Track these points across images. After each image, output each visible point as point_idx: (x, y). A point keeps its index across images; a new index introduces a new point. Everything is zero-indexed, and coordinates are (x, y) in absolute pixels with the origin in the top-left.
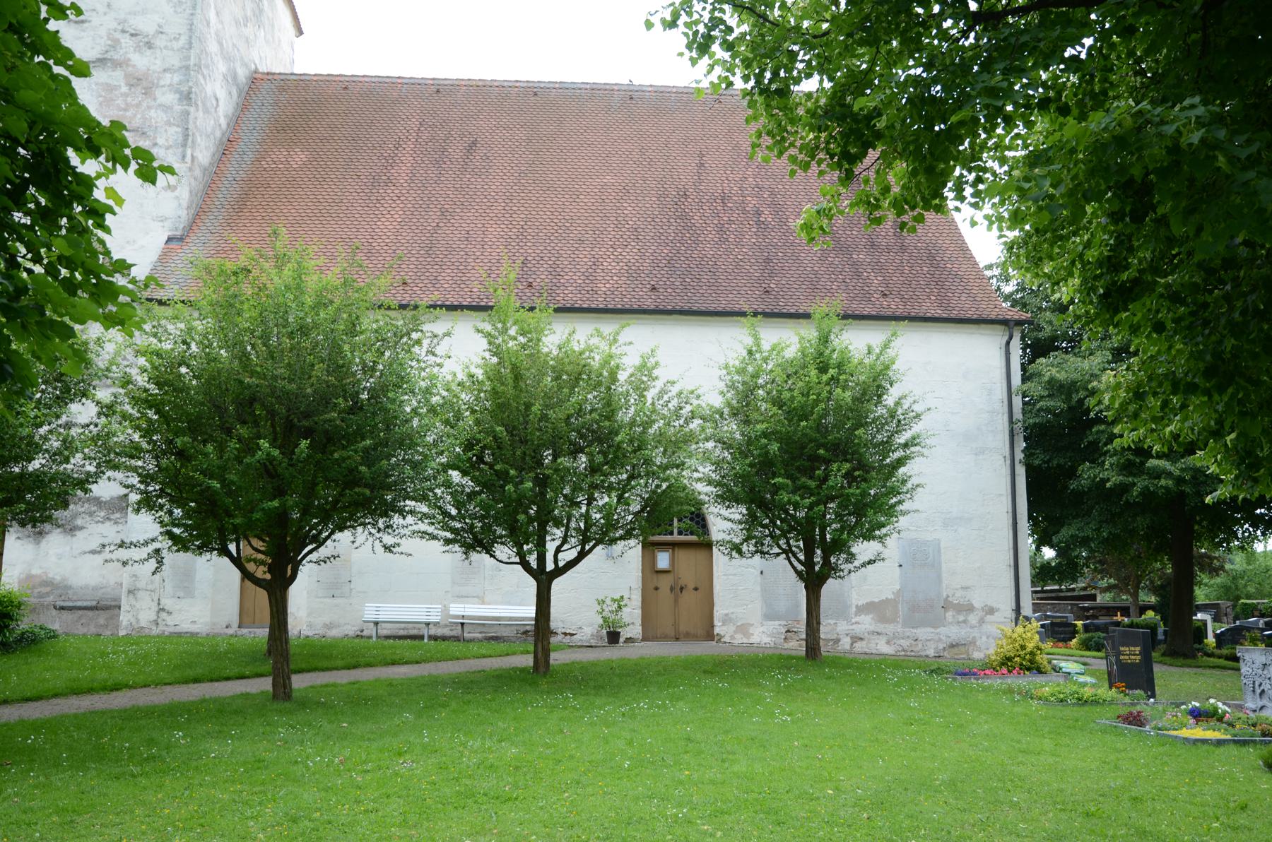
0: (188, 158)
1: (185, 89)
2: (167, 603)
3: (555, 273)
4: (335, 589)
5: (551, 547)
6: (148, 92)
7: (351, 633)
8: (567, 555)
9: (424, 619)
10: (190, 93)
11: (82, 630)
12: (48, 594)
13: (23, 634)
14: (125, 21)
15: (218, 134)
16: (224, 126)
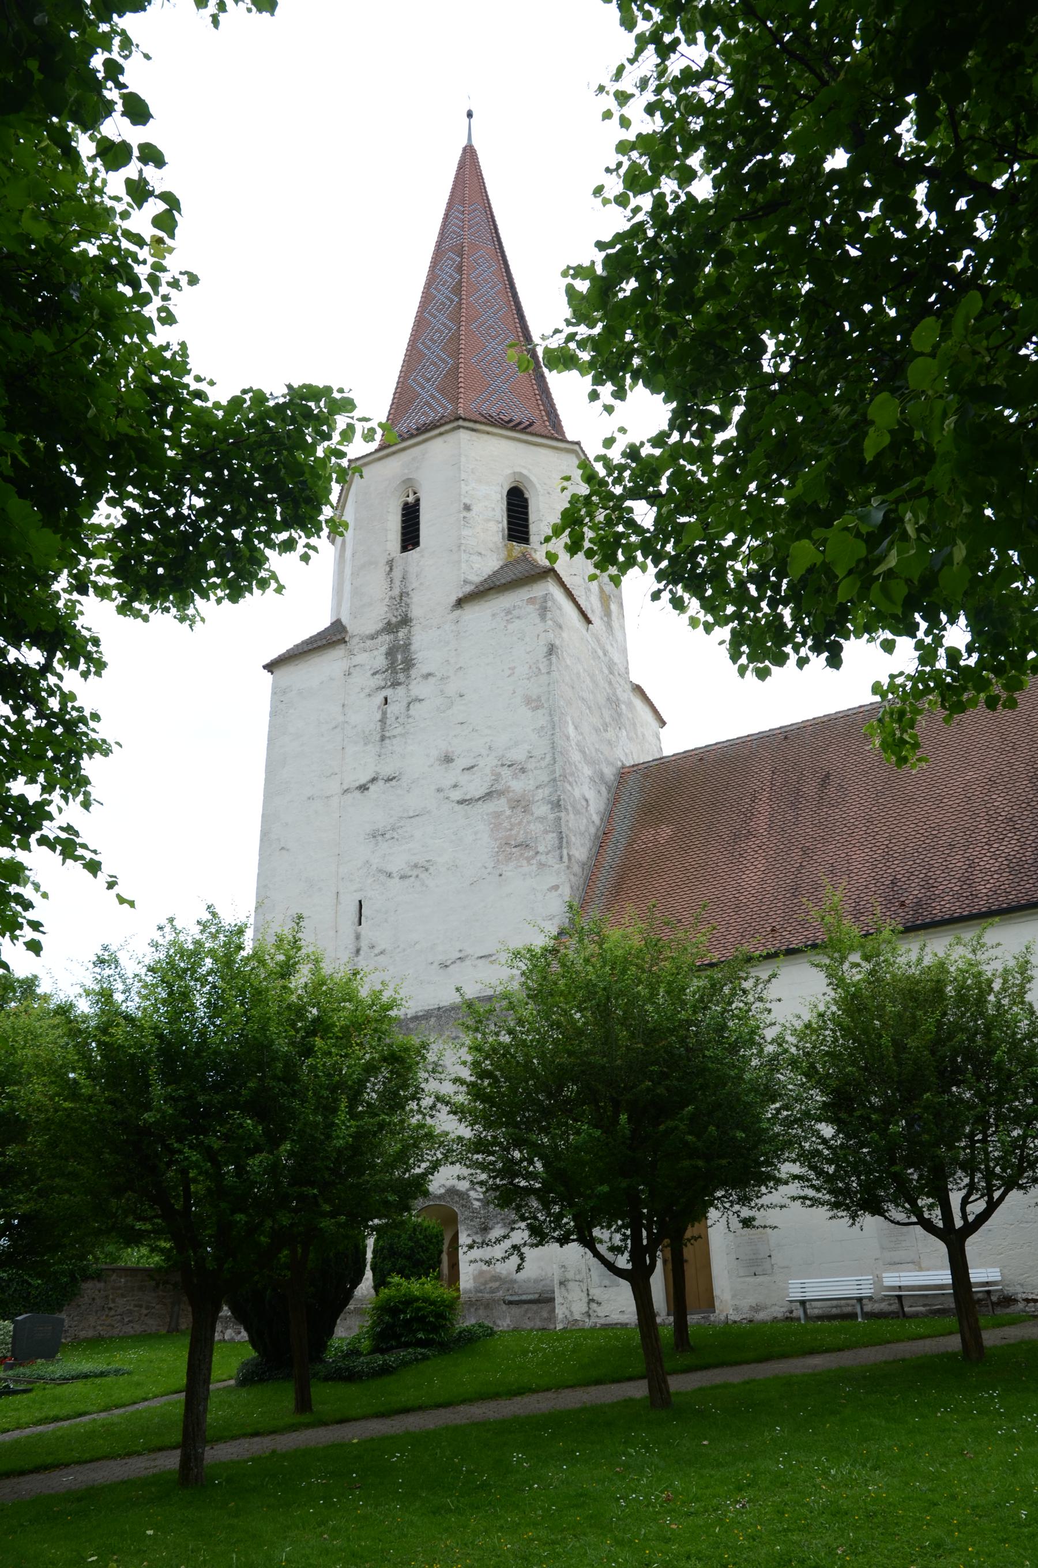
0: (565, 858)
1: (554, 798)
2: (596, 1293)
3: (928, 885)
4: (756, 1265)
5: (955, 1198)
6: (526, 810)
7: (780, 1315)
8: (977, 1207)
9: (855, 1293)
10: (559, 801)
11: (529, 1325)
12: (498, 1289)
13: (460, 1332)
15: (593, 830)
16: (597, 822)
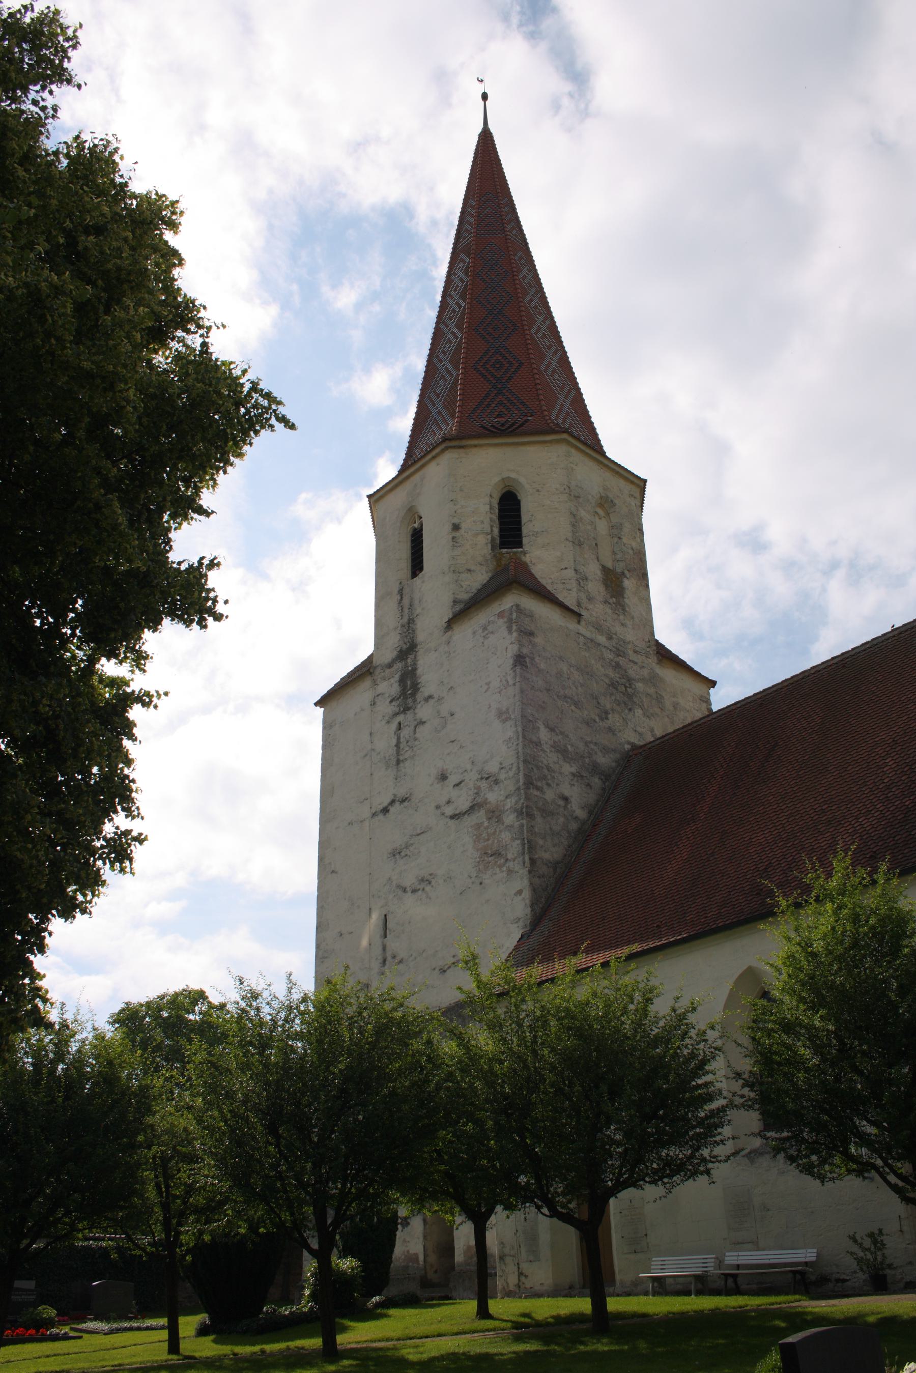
14: (483, 770)
